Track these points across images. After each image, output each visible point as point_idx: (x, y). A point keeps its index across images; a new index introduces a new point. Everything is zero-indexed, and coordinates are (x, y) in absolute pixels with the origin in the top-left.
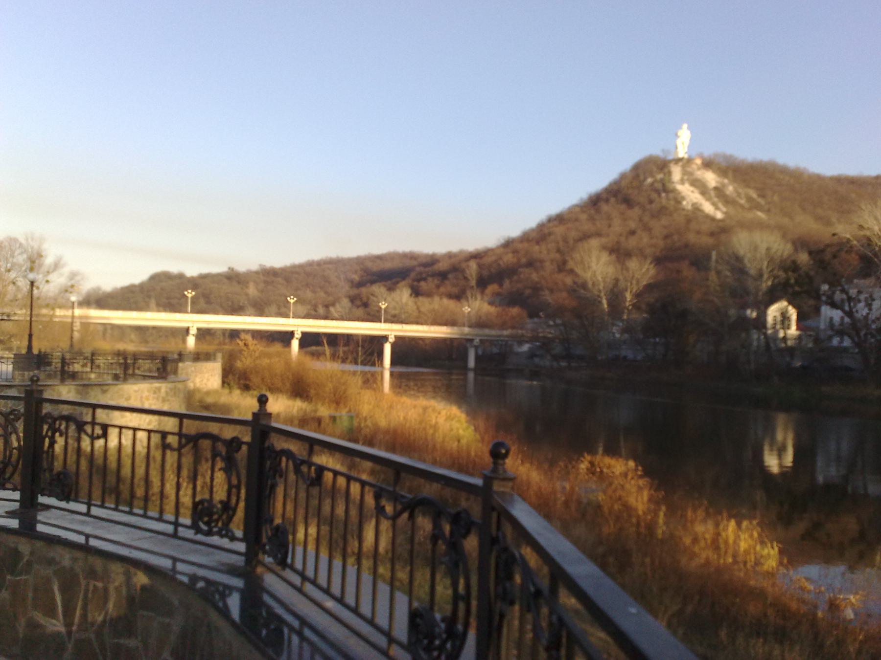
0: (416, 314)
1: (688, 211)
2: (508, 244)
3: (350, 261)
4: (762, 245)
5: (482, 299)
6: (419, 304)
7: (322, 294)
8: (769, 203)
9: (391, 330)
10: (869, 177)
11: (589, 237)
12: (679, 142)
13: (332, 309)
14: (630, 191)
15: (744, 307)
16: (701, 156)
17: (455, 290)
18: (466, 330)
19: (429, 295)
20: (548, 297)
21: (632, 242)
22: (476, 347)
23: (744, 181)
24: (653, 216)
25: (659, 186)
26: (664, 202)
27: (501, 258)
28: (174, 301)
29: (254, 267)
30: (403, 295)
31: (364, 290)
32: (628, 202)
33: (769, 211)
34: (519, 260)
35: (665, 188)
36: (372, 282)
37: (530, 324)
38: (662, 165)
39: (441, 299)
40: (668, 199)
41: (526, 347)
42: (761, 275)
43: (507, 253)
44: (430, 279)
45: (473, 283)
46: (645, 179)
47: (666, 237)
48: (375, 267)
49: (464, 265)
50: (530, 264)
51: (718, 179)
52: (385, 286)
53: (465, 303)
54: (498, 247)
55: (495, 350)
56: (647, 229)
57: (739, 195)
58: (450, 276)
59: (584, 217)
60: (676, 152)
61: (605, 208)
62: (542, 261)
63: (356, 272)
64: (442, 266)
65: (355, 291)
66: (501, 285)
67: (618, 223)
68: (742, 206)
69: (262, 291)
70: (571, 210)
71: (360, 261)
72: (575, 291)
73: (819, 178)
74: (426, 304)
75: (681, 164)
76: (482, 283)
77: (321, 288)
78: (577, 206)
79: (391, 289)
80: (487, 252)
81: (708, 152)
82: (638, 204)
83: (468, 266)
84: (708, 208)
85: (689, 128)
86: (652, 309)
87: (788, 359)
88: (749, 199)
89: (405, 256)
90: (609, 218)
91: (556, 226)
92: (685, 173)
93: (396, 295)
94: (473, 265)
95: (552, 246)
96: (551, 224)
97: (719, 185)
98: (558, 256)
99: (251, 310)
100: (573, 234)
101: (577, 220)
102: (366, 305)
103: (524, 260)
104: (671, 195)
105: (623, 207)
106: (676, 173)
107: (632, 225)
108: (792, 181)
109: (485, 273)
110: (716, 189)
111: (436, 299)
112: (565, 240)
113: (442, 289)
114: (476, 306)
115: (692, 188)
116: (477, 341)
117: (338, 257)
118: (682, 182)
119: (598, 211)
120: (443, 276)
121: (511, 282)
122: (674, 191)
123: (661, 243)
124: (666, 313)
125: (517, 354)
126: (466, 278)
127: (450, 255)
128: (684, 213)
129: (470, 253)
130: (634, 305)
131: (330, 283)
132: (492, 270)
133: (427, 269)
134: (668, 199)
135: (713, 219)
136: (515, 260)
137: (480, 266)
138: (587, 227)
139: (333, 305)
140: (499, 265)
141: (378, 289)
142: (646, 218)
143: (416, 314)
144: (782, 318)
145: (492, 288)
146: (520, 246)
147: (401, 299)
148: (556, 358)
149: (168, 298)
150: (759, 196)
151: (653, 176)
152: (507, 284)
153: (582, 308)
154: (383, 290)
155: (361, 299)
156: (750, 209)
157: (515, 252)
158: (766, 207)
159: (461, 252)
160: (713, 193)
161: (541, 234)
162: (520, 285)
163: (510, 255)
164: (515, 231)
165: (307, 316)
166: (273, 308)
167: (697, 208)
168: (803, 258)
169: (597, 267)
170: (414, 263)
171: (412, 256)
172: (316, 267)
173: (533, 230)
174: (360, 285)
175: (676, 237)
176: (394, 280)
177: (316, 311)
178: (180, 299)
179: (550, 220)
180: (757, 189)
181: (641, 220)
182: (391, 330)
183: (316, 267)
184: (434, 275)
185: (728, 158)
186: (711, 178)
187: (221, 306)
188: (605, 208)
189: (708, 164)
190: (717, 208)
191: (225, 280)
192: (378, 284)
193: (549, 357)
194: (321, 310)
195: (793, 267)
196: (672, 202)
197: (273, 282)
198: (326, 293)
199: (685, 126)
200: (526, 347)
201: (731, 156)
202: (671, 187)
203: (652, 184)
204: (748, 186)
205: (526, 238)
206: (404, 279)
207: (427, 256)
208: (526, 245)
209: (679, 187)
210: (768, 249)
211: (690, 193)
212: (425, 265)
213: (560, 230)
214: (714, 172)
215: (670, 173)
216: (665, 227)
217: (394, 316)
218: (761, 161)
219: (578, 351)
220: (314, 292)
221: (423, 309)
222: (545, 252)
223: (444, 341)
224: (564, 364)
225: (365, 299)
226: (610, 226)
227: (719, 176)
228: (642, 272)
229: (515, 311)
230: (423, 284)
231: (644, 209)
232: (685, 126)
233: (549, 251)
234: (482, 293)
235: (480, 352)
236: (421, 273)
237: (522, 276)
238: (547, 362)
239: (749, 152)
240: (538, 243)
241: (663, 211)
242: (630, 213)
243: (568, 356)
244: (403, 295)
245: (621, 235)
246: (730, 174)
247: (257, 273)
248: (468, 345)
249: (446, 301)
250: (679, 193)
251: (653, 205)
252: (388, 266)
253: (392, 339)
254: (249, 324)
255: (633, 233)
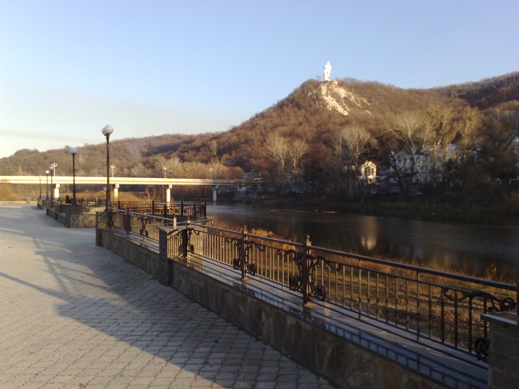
0: (183, 172)
1: (330, 111)
2: (234, 130)
3: (141, 140)
4: (354, 135)
5: (220, 162)
6: (185, 166)
7: (125, 161)
8: (373, 106)
9: (171, 182)
10: (426, 90)
11: (278, 126)
12: (325, 72)
13: (133, 170)
14: (299, 100)
15: (349, 165)
16: (337, 79)
17: (205, 158)
18: (212, 181)
19: (190, 161)
20: (254, 162)
21: (300, 130)
22: (217, 190)
23: (360, 93)
24: (311, 114)
25: (314, 97)
26: (317, 106)
27: (230, 139)
28: (33, 168)
29: (81, 145)
30: (175, 162)
31: (151, 158)
32: (298, 106)
33: (373, 110)
34: (240, 140)
35: (318, 98)
36: (156, 153)
37: (246, 176)
38: (315, 85)
39: (197, 163)
40: (319, 104)
41: (244, 189)
42: (355, 149)
43: (233, 136)
44: (190, 151)
45: (215, 153)
46: (307, 93)
47: (318, 126)
48: (156, 144)
49: (209, 143)
50: (246, 142)
51: (346, 93)
52: (164, 156)
53: (211, 166)
54: (228, 132)
55: (228, 191)
56: (309, 122)
57: (357, 101)
58: (201, 149)
59: (275, 115)
60: (325, 78)
61: (286, 109)
62: (252, 140)
63: (145, 147)
64: (197, 143)
65: (146, 159)
66: (230, 154)
67: (293, 119)
68: (358, 108)
69: (87, 160)
70: (268, 110)
71: (148, 140)
72: (267, 158)
73: (401, 90)
74: (189, 166)
75: (326, 84)
76: (220, 153)
77: (124, 157)
78: (272, 108)
79: (168, 158)
80: (223, 134)
81: (341, 77)
82: (304, 107)
83: (212, 144)
84: (340, 109)
85: (330, 64)
86: (306, 166)
87: (368, 190)
88: (363, 103)
89: (174, 137)
90: (288, 115)
91: (260, 120)
92: (328, 89)
93: (171, 161)
94: (214, 142)
95: (258, 132)
96: (257, 119)
97: (346, 96)
98: (261, 137)
99: (82, 172)
100: (269, 125)
101: (271, 117)
102: (153, 167)
103: (243, 140)
104: (321, 102)
105: (296, 109)
106: (324, 89)
107: (301, 119)
108: (386, 93)
109: (221, 147)
110: (345, 98)
111: (194, 163)
112: (265, 128)
113: (197, 157)
114: (217, 167)
115: (332, 98)
116: (217, 187)
117: (133, 138)
118: (327, 95)
119: (283, 111)
120: (198, 149)
121: (236, 152)
122: (323, 100)
123: (315, 130)
124: (314, 168)
125: (239, 192)
126: (210, 150)
127: (201, 136)
128: (328, 112)
129: (213, 135)
130: (297, 165)
131: (129, 154)
132: (225, 145)
133: (188, 145)
134: (319, 104)
135: (342, 116)
136: (238, 140)
137: (218, 143)
138: (277, 121)
139: (133, 167)
140: (229, 142)
141: (160, 158)
142: (308, 116)
143: (183, 172)
144: (370, 171)
145: (226, 156)
146: (240, 131)
147: (174, 163)
148: (259, 194)
149: (29, 166)
150: (368, 101)
151: (311, 92)
152: (234, 153)
153: (272, 166)
154: (163, 158)
155: (150, 164)
156: (363, 109)
157: (238, 135)
158: (371, 108)
159: (208, 134)
160: (343, 101)
161: (251, 125)
162: (241, 154)
163: (235, 137)
164: (238, 123)
165: (123, 176)
166: (96, 170)
167: (334, 109)
168: (375, 141)
169: (278, 146)
170: (181, 141)
171: (178, 137)
172: (120, 144)
173: (248, 122)
174: (148, 155)
175: (322, 126)
176: (169, 152)
177: (122, 171)
178: (37, 166)
179: (257, 116)
180: (367, 98)
181: (305, 117)
182: (171, 182)
183: (120, 144)
184: (192, 149)
185: (352, 80)
186: (342, 92)
187: (63, 169)
188: (286, 109)
189: (341, 84)
190: (345, 109)
191: (64, 154)
192: (160, 154)
193: (256, 194)
194: (126, 171)
195: (368, 145)
196: (321, 107)
197: (93, 154)
198: (127, 160)
199: (328, 63)
200: (244, 189)
201: (354, 79)
202: (321, 97)
203: (311, 96)
204: (362, 96)
205: (244, 127)
206: (175, 151)
207: (188, 136)
208: (244, 131)
209: (325, 98)
210: (359, 136)
211: (331, 101)
212: (187, 142)
213: (262, 122)
214: (344, 88)
215: (320, 90)
216: (317, 121)
217: (170, 173)
218: (370, 82)
219: (272, 189)
220: (120, 159)
221: (186, 169)
222: (254, 135)
223: (200, 186)
224: (263, 197)
225: (152, 164)
226: (289, 120)
227: (347, 91)
228: (301, 147)
229: (238, 169)
230: (186, 154)
231: (307, 110)
232: (328, 63)
233: (256, 135)
234: (220, 160)
235: (219, 192)
236: (184, 148)
237: (242, 149)
238: (255, 196)
239: (363, 76)
240: (250, 130)
241: (316, 112)
242: (299, 113)
243: (265, 192)
244: (175, 162)
245: (295, 125)
246: (353, 89)
247: (83, 148)
248: (213, 188)
249: (200, 165)
250: (326, 101)
251: (312, 108)
252: (164, 143)
253: (171, 187)
254: (133, 181)
255: (301, 124)
